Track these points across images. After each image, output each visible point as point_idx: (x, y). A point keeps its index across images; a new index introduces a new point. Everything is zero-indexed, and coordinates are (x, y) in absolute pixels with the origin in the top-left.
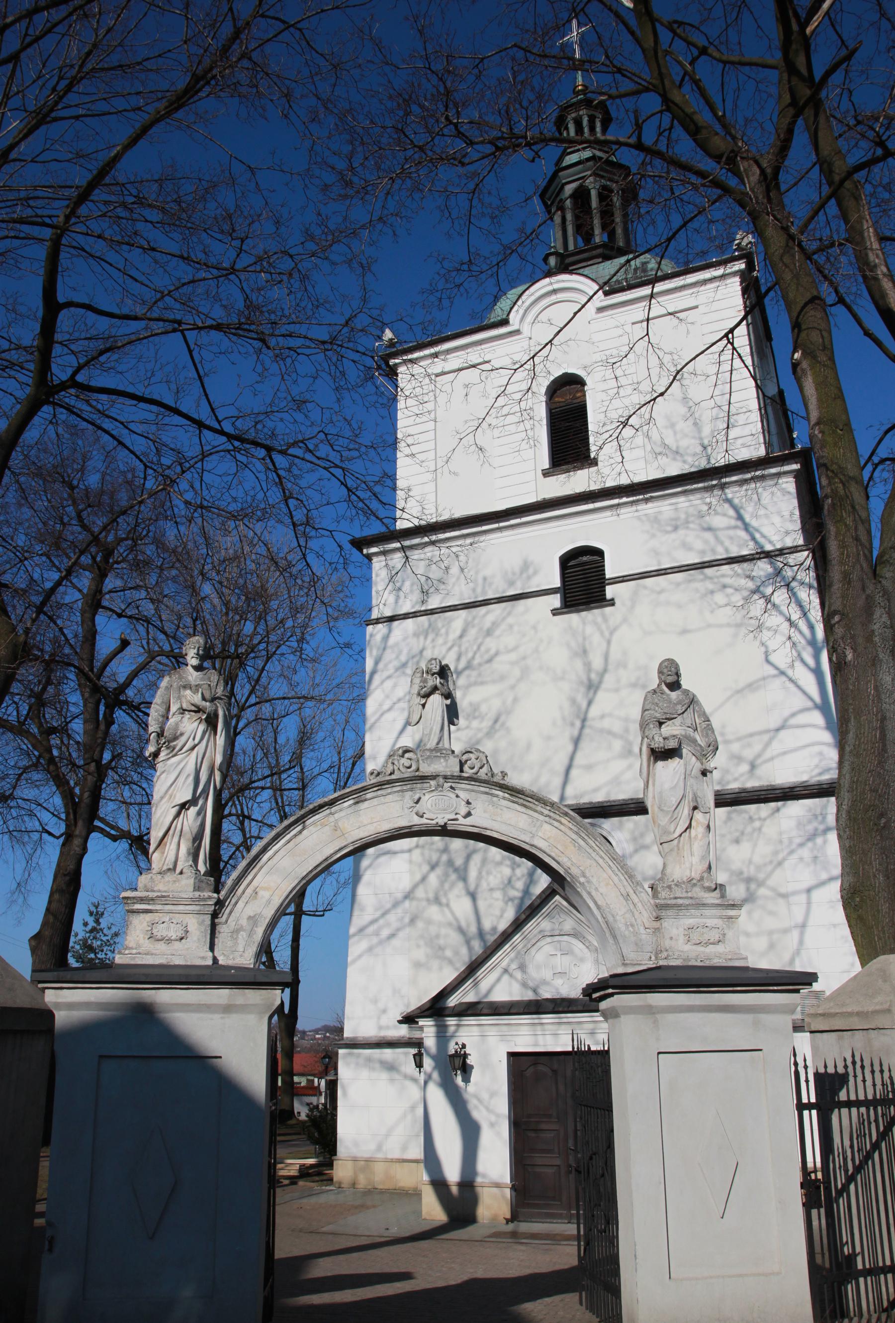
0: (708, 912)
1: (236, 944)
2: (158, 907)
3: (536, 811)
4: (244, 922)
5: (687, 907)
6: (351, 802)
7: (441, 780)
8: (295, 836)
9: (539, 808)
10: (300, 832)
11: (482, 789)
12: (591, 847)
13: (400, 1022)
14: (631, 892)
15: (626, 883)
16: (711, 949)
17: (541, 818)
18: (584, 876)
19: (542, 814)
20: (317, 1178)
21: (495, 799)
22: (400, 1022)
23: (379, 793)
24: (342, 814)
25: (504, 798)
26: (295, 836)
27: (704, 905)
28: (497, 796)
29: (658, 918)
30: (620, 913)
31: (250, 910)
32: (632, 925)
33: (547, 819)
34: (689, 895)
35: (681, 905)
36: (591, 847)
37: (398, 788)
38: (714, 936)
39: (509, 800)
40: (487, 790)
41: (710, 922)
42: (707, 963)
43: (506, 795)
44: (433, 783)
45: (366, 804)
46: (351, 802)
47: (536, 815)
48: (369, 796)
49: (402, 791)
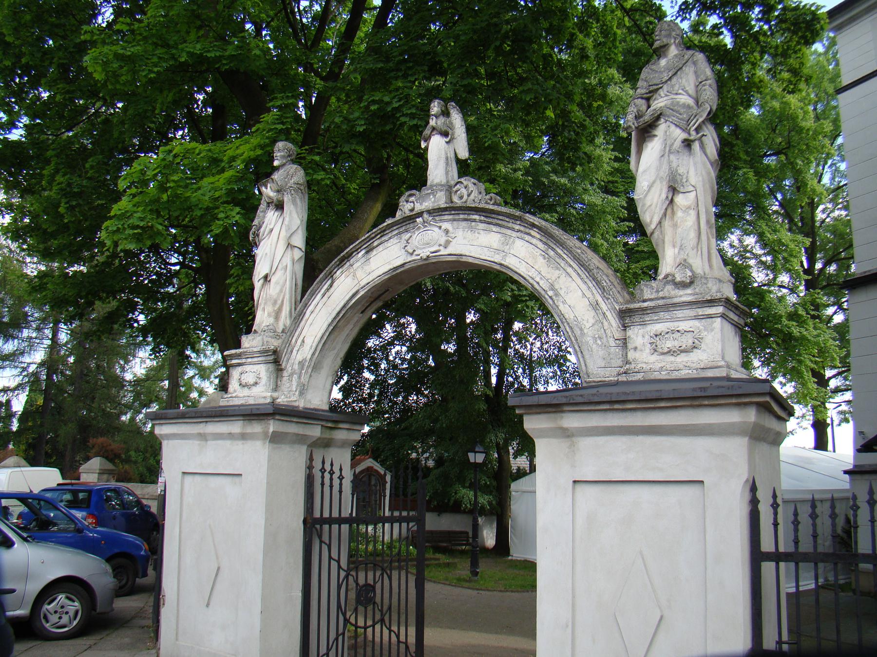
0: (679, 314)
1: (291, 385)
2: (244, 361)
3: (509, 228)
4: (296, 367)
5: (654, 310)
6: (363, 252)
7: (425, 216)
8: (328, 290)
9: (510, 225)
10: (331, 286)
11: (462, 216)
12: (560, 256)
13: (846, 472)
14: (600, 299)
15: (595, 291)
16: (682, 359)
17: (514, 234)
18: (552, 290)
19: (513, 229)
20: (467, 584)
21: (473, 224)
22: (846, 472)
23: (383, 239)
24: (359, 264)
25: (481, 221)
26: (328, 290)
27: (674, 305)
28: (474, 220)
29: (625, 327)
30: (588, 325)
31: (300, 358)
32: (600, 338)
33: (519, 234)
34: (661, 294)
35: (645, 309)
36: (560, 256)
37: (396, 232)
38: (687, 341)
39: (485, 222)
40: (466, 216)
41: (683, 326)
42: (675, 375)
43: (482, 218)
44: (419, 220)
45: (374, 252)
46: (363, 252)
47: (509, 232)
48: (375, 244)
49: (399, 233)
